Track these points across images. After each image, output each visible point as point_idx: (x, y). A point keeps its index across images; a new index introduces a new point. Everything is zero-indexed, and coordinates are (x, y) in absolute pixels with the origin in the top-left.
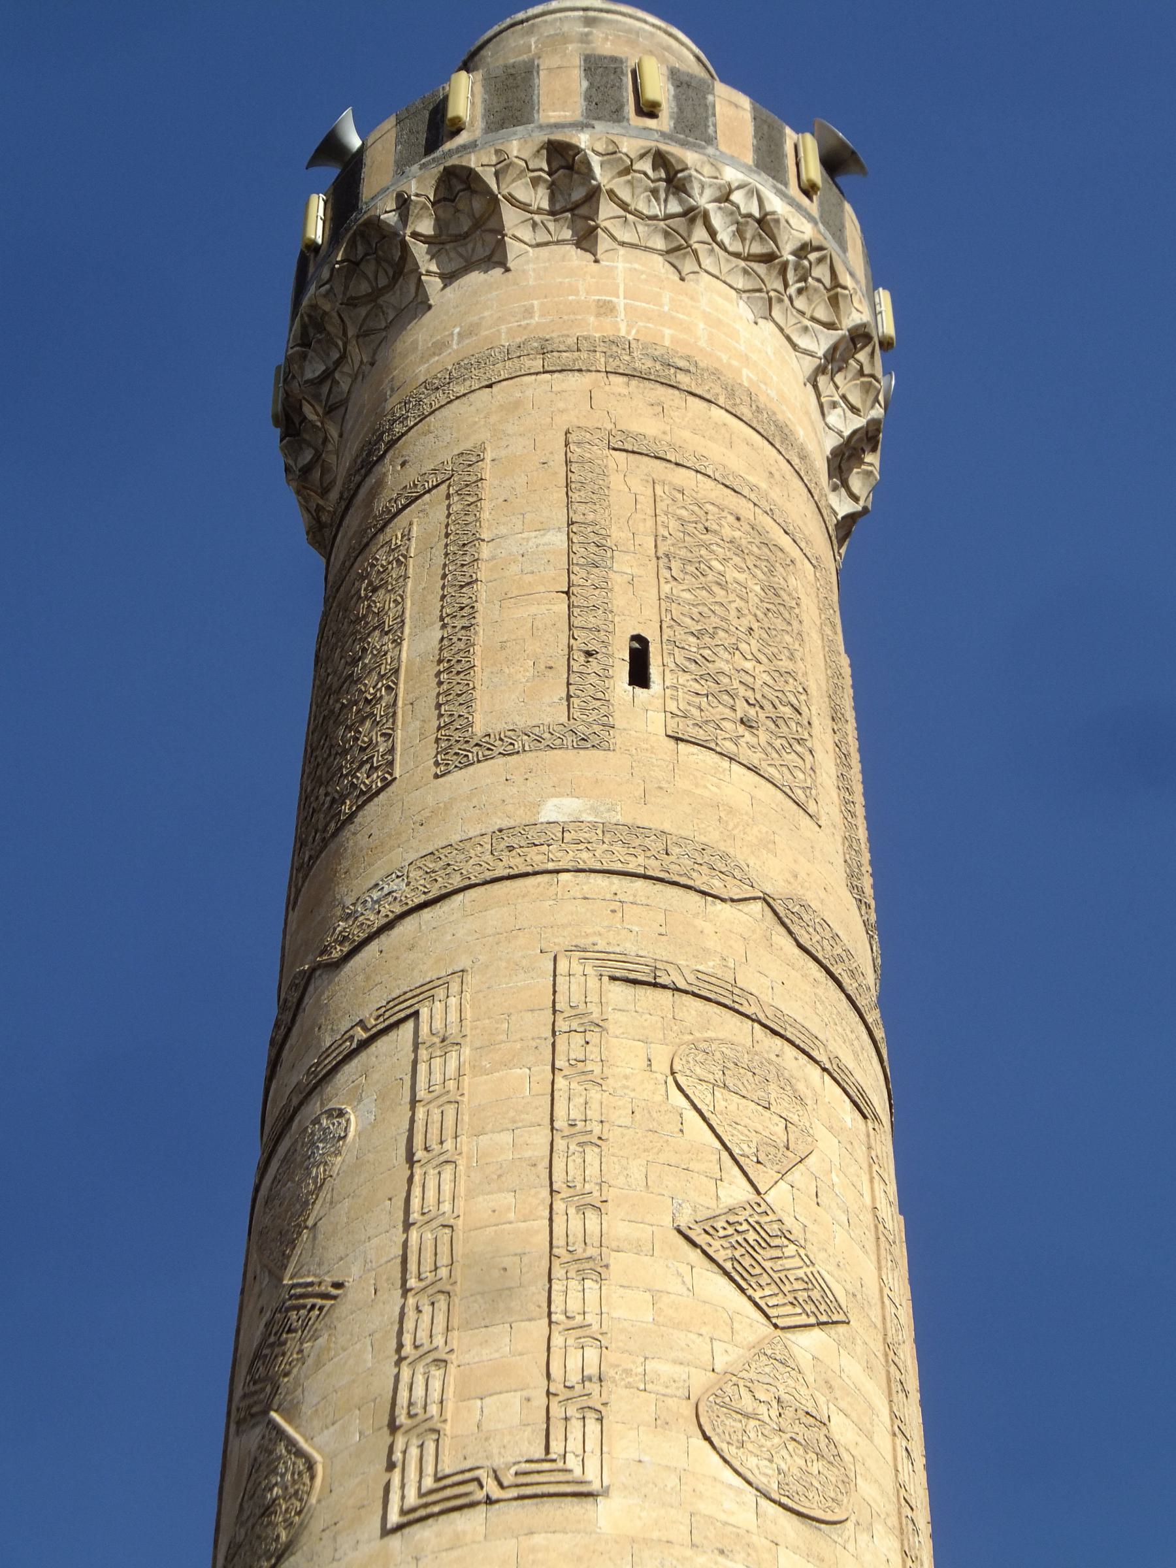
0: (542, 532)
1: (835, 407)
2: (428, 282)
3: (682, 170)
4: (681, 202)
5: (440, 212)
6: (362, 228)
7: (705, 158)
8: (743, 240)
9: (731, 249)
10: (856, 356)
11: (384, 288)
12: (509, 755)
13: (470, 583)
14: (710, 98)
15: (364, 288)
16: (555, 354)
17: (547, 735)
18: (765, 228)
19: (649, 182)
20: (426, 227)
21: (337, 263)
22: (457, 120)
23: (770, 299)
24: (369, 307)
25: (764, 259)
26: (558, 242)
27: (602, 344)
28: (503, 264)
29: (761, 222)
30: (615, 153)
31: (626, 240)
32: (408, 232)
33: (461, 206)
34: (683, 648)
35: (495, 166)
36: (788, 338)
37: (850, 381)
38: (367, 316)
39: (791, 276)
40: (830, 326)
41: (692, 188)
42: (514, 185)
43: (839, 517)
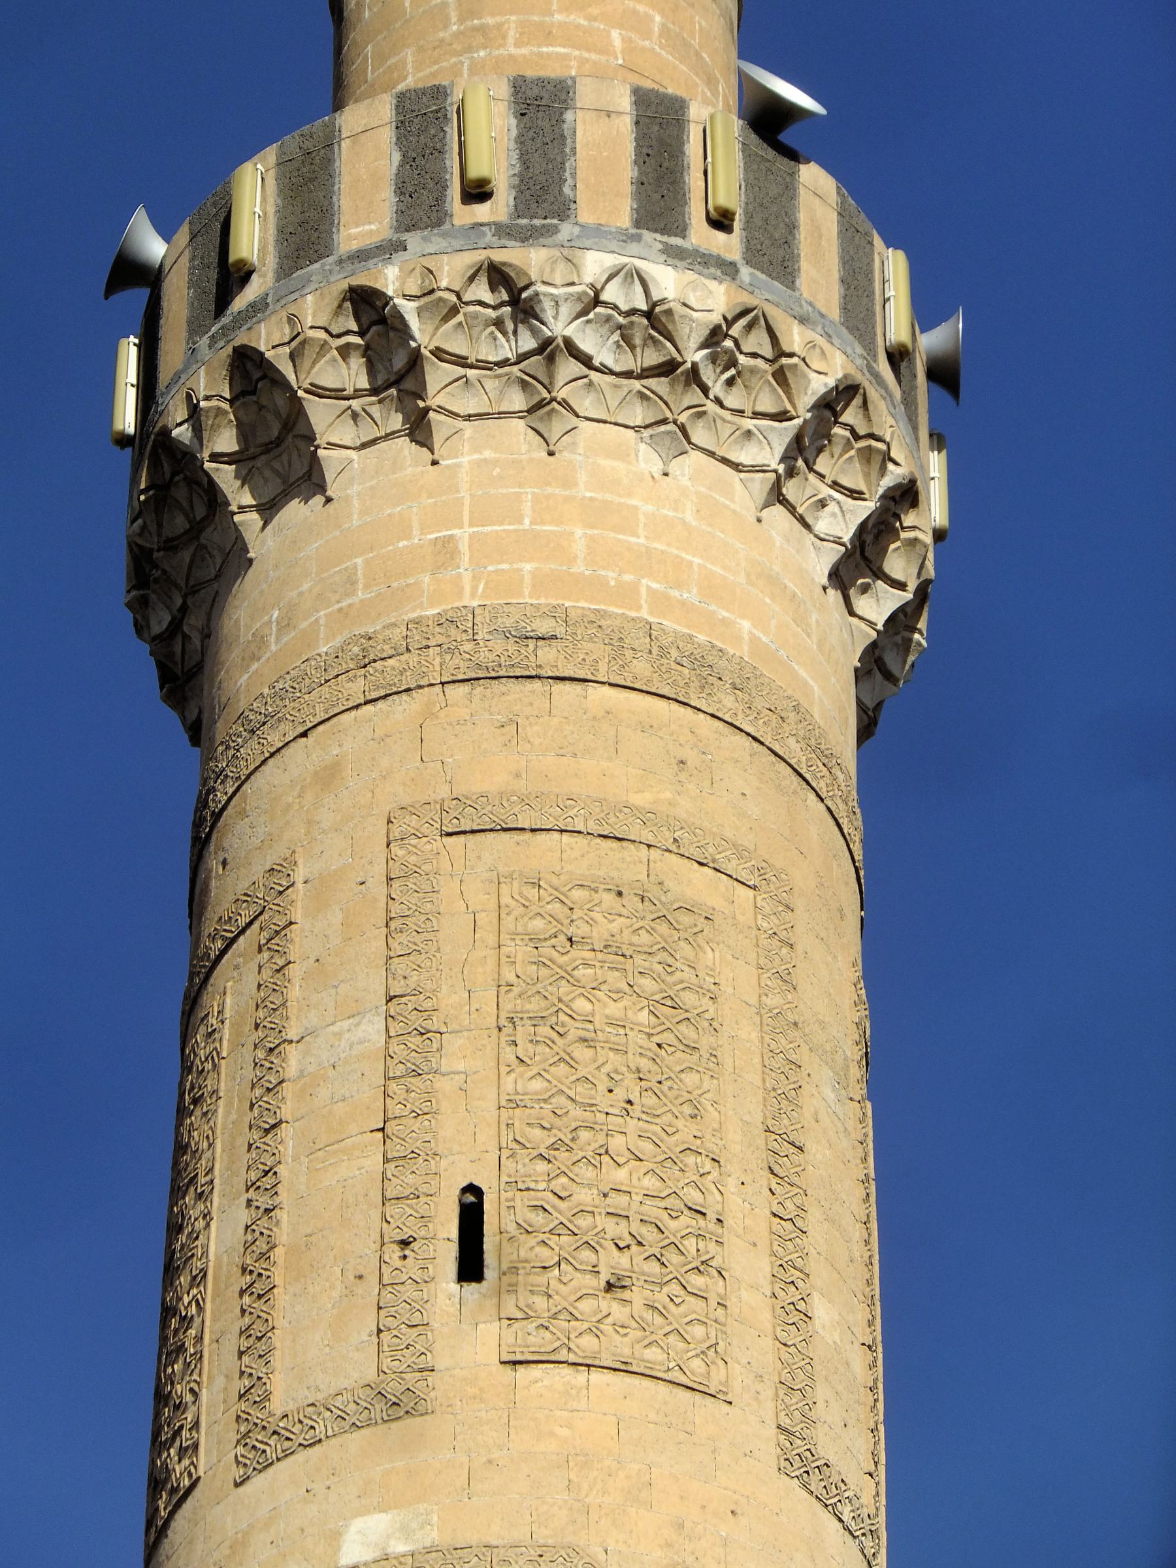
0: (357, 1019)
1: (824, 506)
2: (242, 523)
3: (526, 287)
4: (534, 332)
5: (241, 413)
6: (160, 438)
7: (556, 252)
8: (632, 348)
9: (618, 369)
10: (840, 420)
11: (203, 520)
12: (310, 1445)
13: (274, 1126)
14: (569, 116)
15: (180, 523)
16: (378, 665)
17: (351, 1408)
18: (656, 325)
19: (490, 310)
20: (226, 441)
21: (142, 492)
22: (241, 263)
23: (683, 429)
24: (192, 548)
25: (661, 370)
26: (387, 437)
27: (438, 629)
28: (321, 488)
29: (649, 315)
30: (432, 292)
31: (472, 412)
32: (206, 455)
33: (264, 401)
34: (528, 1189)
35: (289, 343)
36: (725, 461)
37: (841, 455)
38: (192, 561)
39: (707, 374)
40: (782, 416)
41: (543, 310)
42: (318, 366)
43: (880, 627)
